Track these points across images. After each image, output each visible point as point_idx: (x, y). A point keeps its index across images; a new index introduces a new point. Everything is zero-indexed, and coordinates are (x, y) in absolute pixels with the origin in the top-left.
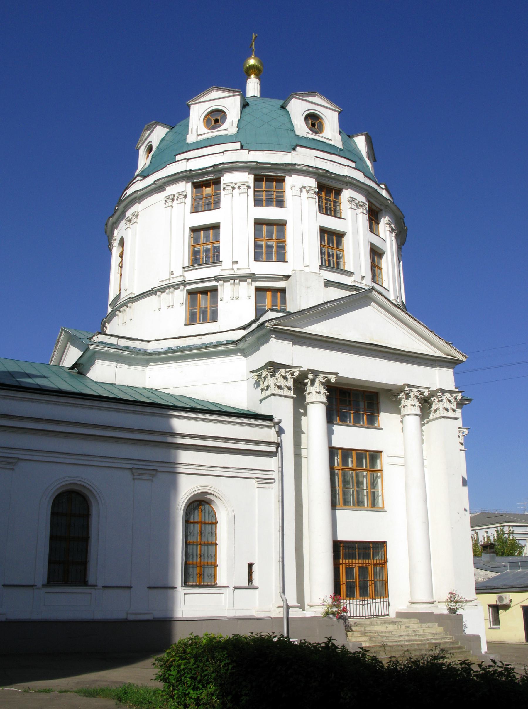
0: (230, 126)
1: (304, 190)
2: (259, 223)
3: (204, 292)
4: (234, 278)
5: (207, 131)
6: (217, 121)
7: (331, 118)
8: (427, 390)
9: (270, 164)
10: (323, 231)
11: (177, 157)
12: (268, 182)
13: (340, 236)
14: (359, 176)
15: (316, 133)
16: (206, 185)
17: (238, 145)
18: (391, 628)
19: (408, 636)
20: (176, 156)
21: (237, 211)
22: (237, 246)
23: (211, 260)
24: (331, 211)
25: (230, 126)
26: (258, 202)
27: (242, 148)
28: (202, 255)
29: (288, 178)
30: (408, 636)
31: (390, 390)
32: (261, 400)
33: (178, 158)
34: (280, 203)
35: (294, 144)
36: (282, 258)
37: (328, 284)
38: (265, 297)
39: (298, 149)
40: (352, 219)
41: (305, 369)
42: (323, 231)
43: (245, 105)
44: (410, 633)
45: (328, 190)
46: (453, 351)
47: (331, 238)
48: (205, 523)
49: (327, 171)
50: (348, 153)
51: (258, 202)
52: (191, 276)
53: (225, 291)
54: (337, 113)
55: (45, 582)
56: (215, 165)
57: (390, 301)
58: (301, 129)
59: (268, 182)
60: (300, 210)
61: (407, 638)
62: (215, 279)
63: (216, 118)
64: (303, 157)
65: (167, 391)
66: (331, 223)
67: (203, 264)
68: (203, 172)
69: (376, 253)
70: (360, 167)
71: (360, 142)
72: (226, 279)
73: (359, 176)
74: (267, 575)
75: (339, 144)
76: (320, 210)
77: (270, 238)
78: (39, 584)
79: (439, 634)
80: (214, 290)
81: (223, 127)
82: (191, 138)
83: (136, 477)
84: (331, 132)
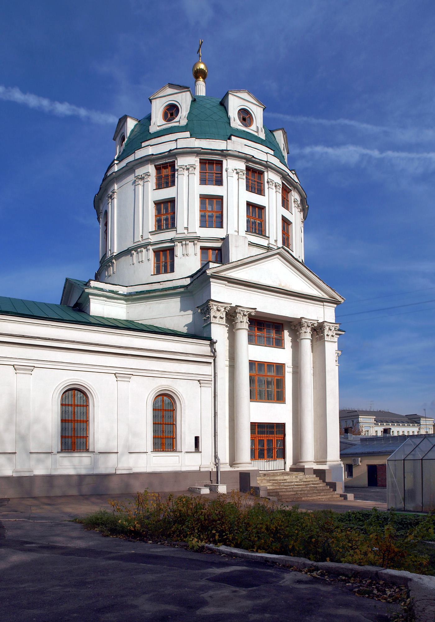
0: (182, 118)
1: (235, 171)
2: (204, 198)
3: (164, 250)
4: (185, 239)
5: (164, 122)
6: (172, 115)
7: (257, 112)
8: (316, 322)
9: (211, 150)
10: (249, 204)
11: (143, 144)
12: (212, 168)
13: (261, 208)
14: (276, 161)
15: (246, 126)
16: (167, 172)
17: (188, 134)
18: (286, 477)
19: (297, 482)
20: (141, 143)
21: (189, 189)
22: (188, 216)
23: (170, 226)
24: (255, 189)
25: (182, 118)
26: (203, 181)
27: (191, 136)
28: (164, 222)
29: (225, 162)
30: (297, 482)
31: (291, 322)
32: (204, 327)
33: (143, 144)
34: (219, 182)
35: (229, 134)
36: (220, 225)
37: (251, 244)
38: (207, 254)
39: (233, 137)
40: (271, 199)
41: (233, 305)
42: (249, 204)
43: (194, 101)
44: (298, 480)
45: (255, 177)
46: (336, 295)
47: (256, 213)
48: (166, 410)
49: (253, 157)
50: (270, 143)
51: (203, 181)
52: (153, 239)
53: (179, 250)
54: (262, 109)
55: (60, 451)
56: (171, 150)
57: (294, 257)
58: (236, 123)
59: (212, 168)
60: (234, 192)
61: (296, 484)
62: (172, 241)
63: (172, 111)
64: (237, 145)
65: (140, 322)
66: (256, 199)
67: (164, 229)
68: (162, 156)
69: (286, 222)
70: (278, 154)
71: (279, 136)
72: (180, 240)
73: (276, 161)
74: (206, 444)
75: (262, 136)
76: (248, 189)
77: (213, 211)
78: (55, 451)
79: (316, 481)
80: (171, 250)
81: (177, 119)
82: (153, 129)
83: (118, 379)
84: (257, 126)
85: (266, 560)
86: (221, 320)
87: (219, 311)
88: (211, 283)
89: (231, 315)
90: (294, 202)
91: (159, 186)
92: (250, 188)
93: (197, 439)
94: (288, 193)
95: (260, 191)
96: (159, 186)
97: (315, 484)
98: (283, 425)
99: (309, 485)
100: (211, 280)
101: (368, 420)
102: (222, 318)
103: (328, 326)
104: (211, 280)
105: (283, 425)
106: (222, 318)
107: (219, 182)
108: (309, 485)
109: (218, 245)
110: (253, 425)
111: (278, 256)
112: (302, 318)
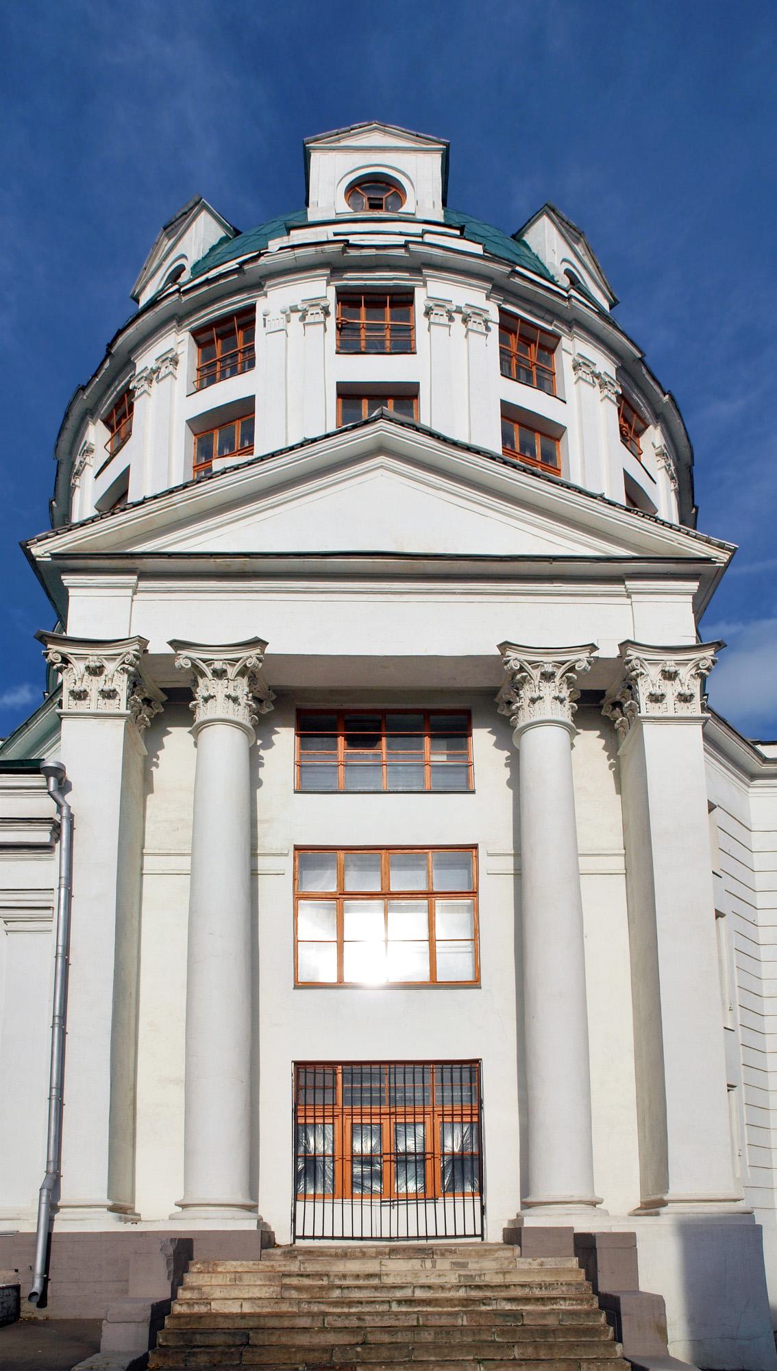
8: (584, 655)
10: (505, 405)
26: (349, 342)
34: (405, 346)
40: (582, 406)
42: (505, 405)
51: (349, 342)
85: (525, 1304)
88: (71, 592)
89: (163, 698)
91: (208, 376)
92: (513, 367)
95: (544, 380)
96: (208, 376)
100: (68, 580)
103: (653, 663)
104: (68, 580)
107: (405, 346)
109: (217, 464)
110: (301, 1067)
112: (505, 646)
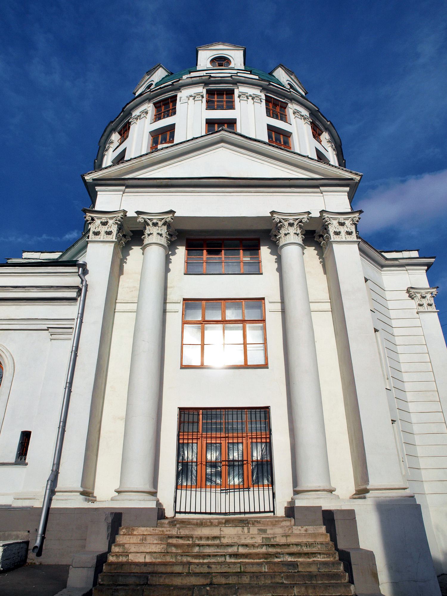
10: (268, 126)
26: (210, 106)
42: (268, 126)
74: (41, 450)
86: (429, 307)
87: (424, 297)
90: (294, 113)
92: (270, 113)
93: (26, 436)
94: (285, 108)
95: (283, 117)
97: (307, 555)
98: (266, 410)
99: (276, 555)
101: (123, 324)
102: (430, 305)
105: (266, 410)
106: (430, 305)
108: (276, 555)
111: (222, 144)
